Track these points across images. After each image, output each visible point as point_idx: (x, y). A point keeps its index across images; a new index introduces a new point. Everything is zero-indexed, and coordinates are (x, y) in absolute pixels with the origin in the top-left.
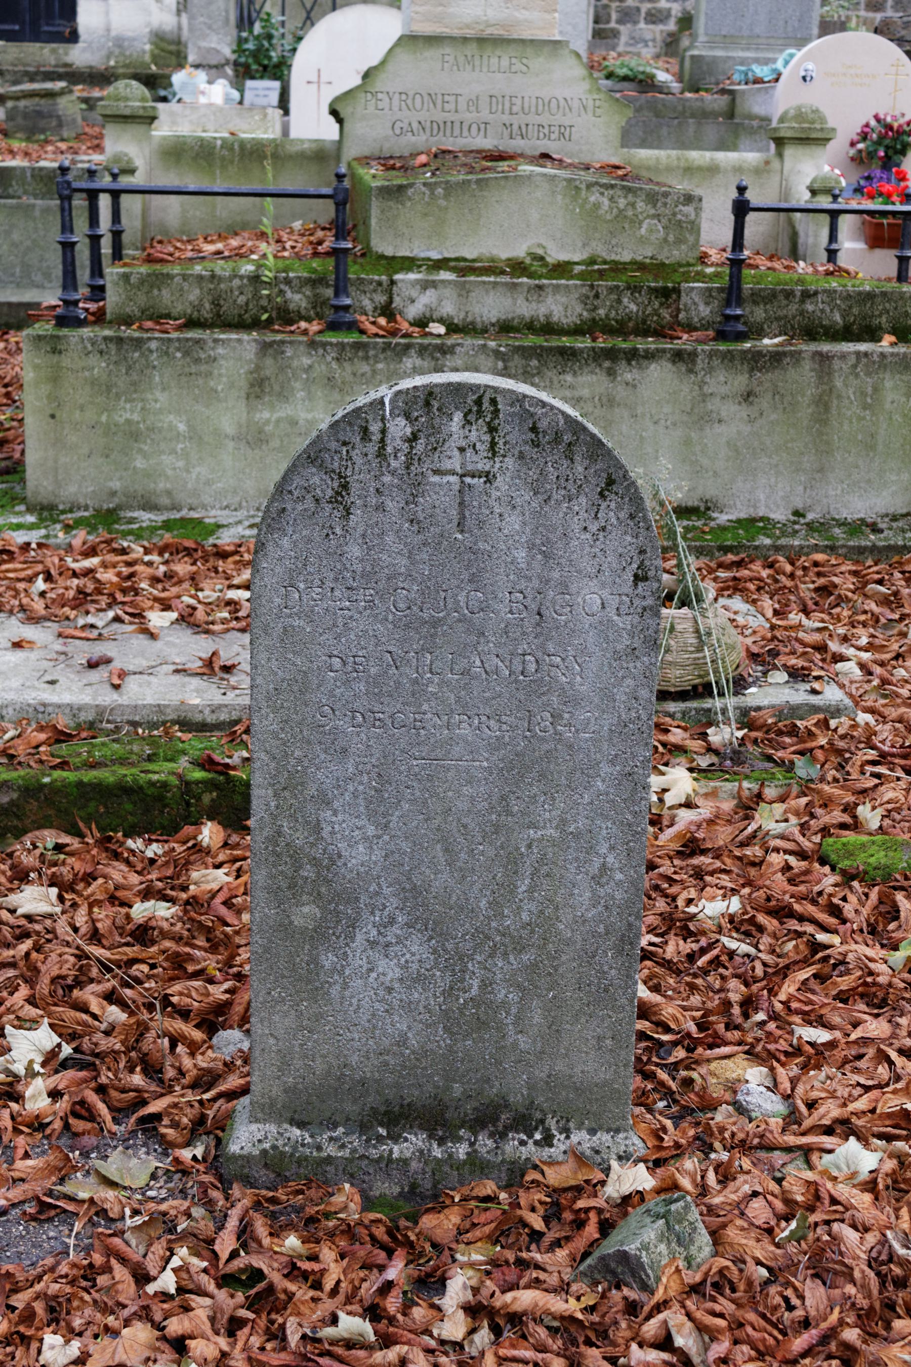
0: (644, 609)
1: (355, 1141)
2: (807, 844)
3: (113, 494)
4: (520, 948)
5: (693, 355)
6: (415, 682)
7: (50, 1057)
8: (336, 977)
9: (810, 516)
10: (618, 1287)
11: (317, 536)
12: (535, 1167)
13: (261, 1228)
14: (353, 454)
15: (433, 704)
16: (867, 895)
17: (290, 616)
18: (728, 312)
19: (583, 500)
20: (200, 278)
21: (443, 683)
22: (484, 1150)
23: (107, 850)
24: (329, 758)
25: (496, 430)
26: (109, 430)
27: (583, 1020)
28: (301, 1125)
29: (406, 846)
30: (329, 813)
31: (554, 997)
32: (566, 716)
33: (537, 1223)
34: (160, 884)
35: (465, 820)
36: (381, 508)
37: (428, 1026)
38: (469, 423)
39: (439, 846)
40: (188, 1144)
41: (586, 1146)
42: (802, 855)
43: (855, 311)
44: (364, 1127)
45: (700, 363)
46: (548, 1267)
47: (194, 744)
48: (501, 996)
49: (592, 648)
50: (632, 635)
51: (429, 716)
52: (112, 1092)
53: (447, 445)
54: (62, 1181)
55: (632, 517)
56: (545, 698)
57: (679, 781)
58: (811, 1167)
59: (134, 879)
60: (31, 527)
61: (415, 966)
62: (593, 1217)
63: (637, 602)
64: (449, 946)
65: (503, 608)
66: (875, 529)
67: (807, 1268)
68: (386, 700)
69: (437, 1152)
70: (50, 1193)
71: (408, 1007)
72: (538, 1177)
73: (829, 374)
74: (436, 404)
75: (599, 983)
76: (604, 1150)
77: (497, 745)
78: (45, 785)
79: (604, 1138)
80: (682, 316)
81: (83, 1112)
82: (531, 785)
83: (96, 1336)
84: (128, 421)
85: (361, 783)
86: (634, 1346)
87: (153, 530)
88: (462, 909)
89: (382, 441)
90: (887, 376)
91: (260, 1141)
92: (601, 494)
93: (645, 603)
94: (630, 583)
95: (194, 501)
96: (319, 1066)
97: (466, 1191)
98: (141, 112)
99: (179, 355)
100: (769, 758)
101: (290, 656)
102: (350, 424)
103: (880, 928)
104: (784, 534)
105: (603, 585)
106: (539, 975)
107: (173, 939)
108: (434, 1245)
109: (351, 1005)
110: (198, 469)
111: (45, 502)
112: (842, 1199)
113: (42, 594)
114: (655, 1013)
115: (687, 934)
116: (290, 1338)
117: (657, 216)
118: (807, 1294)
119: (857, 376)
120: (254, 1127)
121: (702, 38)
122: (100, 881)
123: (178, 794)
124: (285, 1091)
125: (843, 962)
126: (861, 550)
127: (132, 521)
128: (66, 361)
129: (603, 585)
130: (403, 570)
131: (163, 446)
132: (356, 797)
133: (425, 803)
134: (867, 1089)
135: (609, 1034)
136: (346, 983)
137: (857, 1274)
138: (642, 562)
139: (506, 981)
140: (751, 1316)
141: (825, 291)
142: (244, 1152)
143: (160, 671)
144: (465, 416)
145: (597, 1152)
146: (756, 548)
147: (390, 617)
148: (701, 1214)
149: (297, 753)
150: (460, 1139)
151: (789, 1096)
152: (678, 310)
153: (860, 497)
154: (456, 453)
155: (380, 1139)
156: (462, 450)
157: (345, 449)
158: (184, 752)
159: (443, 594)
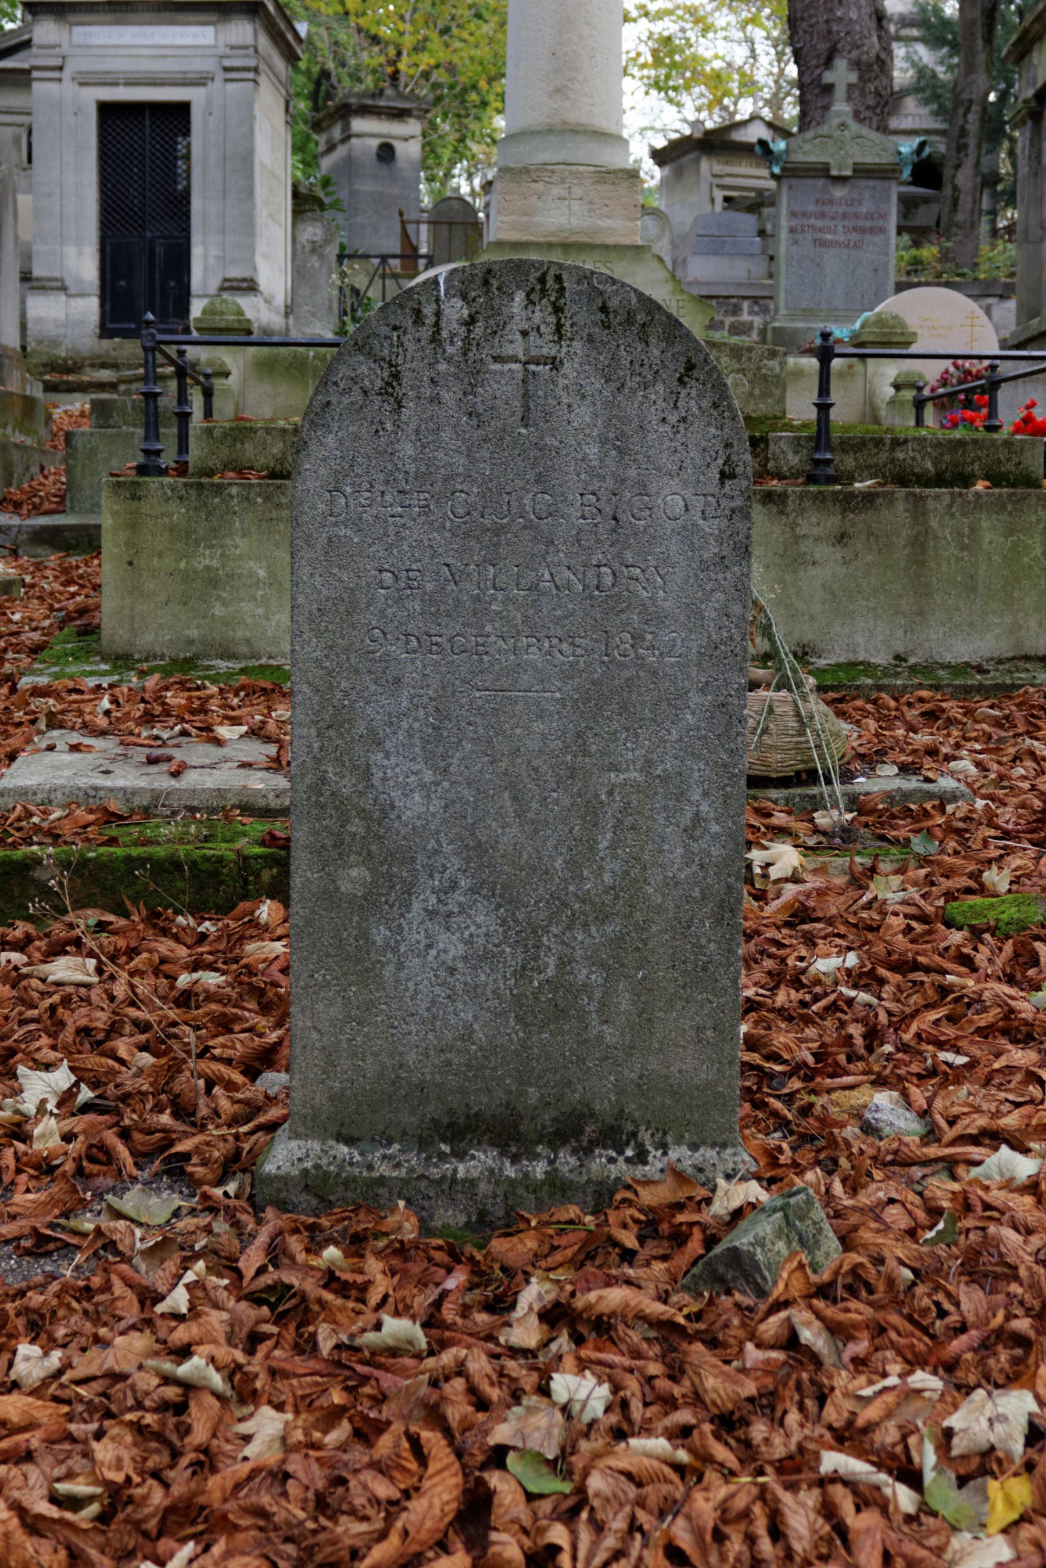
0: (733, 511)
1: (414, 1160)
2: (930, 909)
3: (191, 642)
4: (603, 917)
5: (784, 496)
6: (477, 599)
7: (66, 1098)
8: (390, 955)
9: (912, 660)
10: (729, 1293)
11: (365, 432)
12: (628, 1187)
13: (295, 1244)
14: (405, 339)
15: (497, 625)
16: (1000, 949)
17: (336, 524)
18: (817, 456)
19: (660, 388)
20: (284, 431)
21: (508, 600)
22: (566, 1169)
23: (155, 926)
24: (380, 690)
25: (562, 310)
26: (187, 577)
27: (679, 1007)
28: (350, 1141)
29: (468, 794)
30: (381, 755)
31: (644, 978)
32: (649, 637)
33: (629, 1239)
34: (210, 958)
35: (535, 763)
36: (436, 399)
37: (498, 1015)
38: (532, 303)
39: (506, 794)
40: (220, 1182)
41: (687, 1163)
42: (923, 918)
43: (947, 458)
44: (423, 1143)
45: (792, 504)
46: (643, 1283)
47: (258, 827)
48: (582, 977)
49: (675, 557)
50: (720, 541)
51: (493, 639)
52: (136, 1130)
53: (508, 327)
54: (66, 1215)
55: (715, 406)
56: (624, 616)
57: (785, 857)
58: (954, 1178)
59: (182, 952)
60: (104, 674)
61: (481, 941)
62: (697, 1234)
63: (724, 503)
64: (520, 916)
65: (574, 512)
66: (980, 670)
67: (961, 1274)
68: (444, 621)
69: (510, 1171)
70: (51, 1226)
71: (474, 991)
72: (629, 1195)
73: (924, 514)
74: (495, 283)
75: (696, 960)
76: (708, 1168)
77: (571, 672)
78: (90, 860)
79: (708, 1154)
80: (771, 465)
81: (102, 1157)
82: (611, 719)
83: (84, 1350)
84: (208, 568)
85: (416, 719)
86: (750, 1346)
87: (230, 675)
88: (534, 869)
89: (437, 324)
90: (984, 516)
91: (300, 1160)
92: (680, 380)
93: (733, 505)
94: (716, 481)
95: (273, 650)
96: (370, 1066)
97: (545, 1217)
98: (236, 325)
99: (259, 500)
100: (883, 838)
101: (335, 570)
102: (401, 306)
103: (1019, 976)
104: (886, 675)
105: (685, 484)
106: (625, 950)
107: (220, 1001)
108: (503, 1269)
109: (407, 989)
110: (277, 617)
111: (120, 651)
112: (997, 1203)
113: (107, 713)
114: (765, 1045)
115: (797, 983)
116: (321, 1344)
117: (742, 371)
118: (963, 1298)
119: (952, 516)
120: (294, 1144)
121: (783, 311)
122: (145, 955)
123: (235, 869)
124: (331, 1099)
125: (980, 1001)
126: (968, 690)
127: (208, 668)
128: (145, 507)
129: (685, 484)
130: (461, 470)
131: (242, 593)
132: (411, 736)
133: (490, 742)
134: (1017, 1105)
135: (710, 1023)
136: (400, 963)
137: (1023, 1273)
138: (728, 458)
139: (587, 958)
140: (895, 1319)
141: (915, 439)
142: (282, 1172)
143: (226, 766)
144: (528, 295)
145: (701, 1170)
146: (858, 687)
147: (448, 524)
148: (828, 1216)
149: (344, 684)
150: (536, 1157)
151: (925, 1112)
152: (767, 459)
153: (966, 641)
154: (518, 336)
155: (442, 1157)
156: (525, 334)
157: (395, 334)
158: (244, 834)
159: (506, 498)
